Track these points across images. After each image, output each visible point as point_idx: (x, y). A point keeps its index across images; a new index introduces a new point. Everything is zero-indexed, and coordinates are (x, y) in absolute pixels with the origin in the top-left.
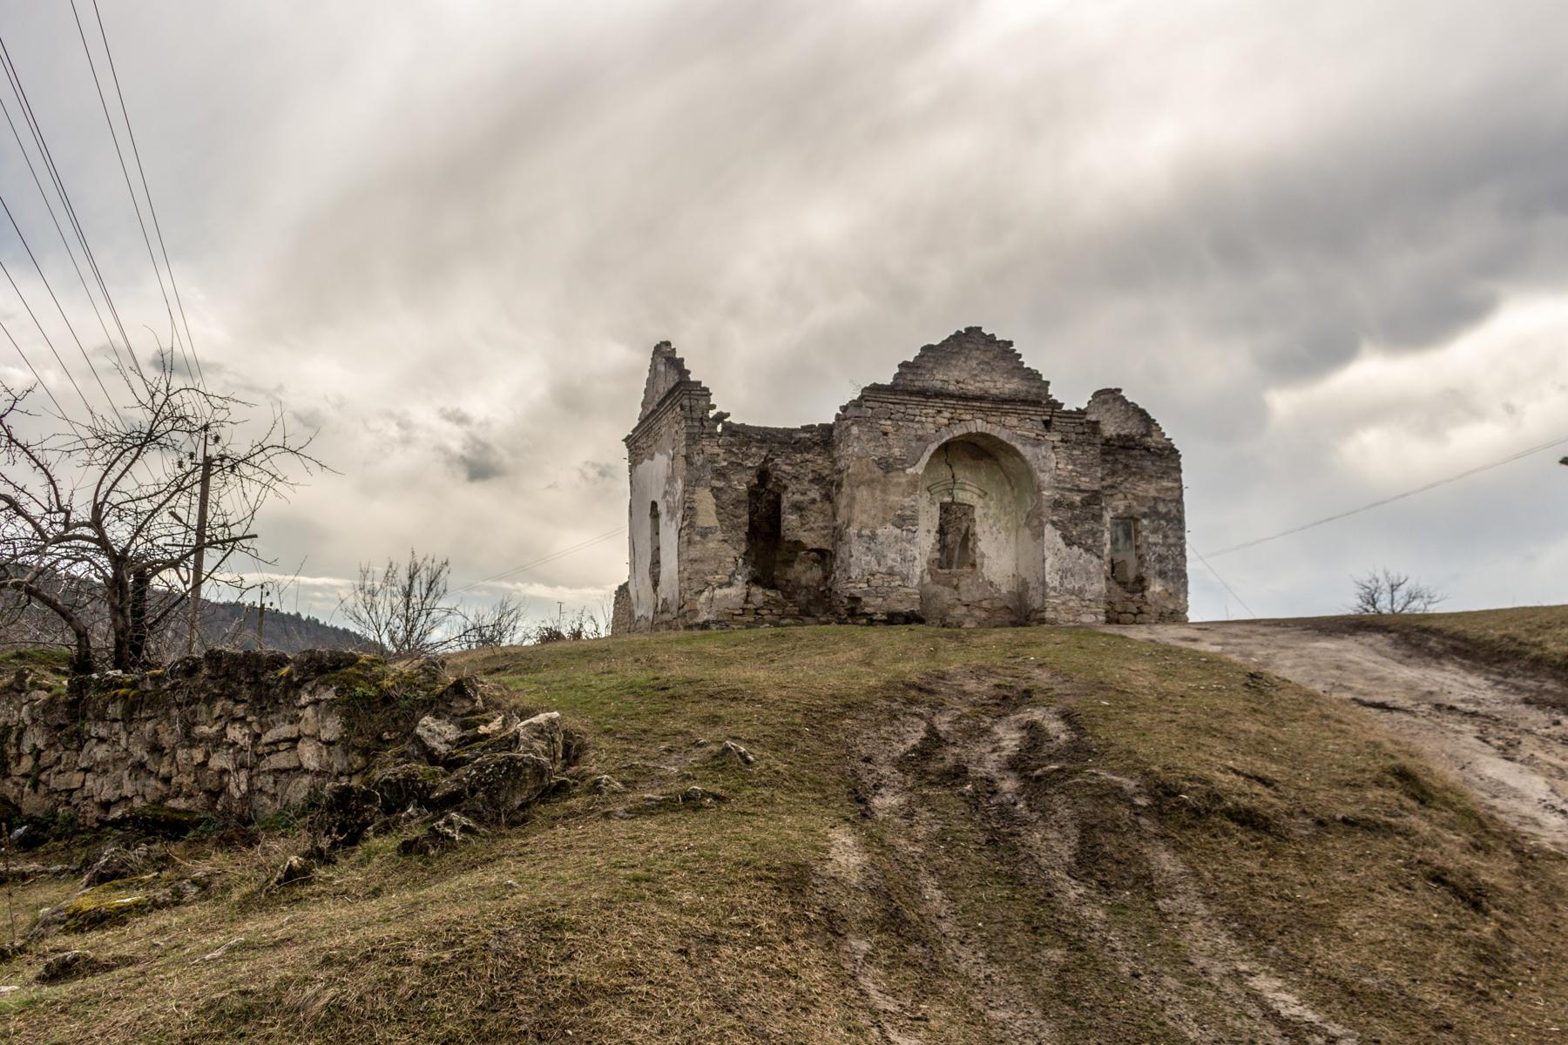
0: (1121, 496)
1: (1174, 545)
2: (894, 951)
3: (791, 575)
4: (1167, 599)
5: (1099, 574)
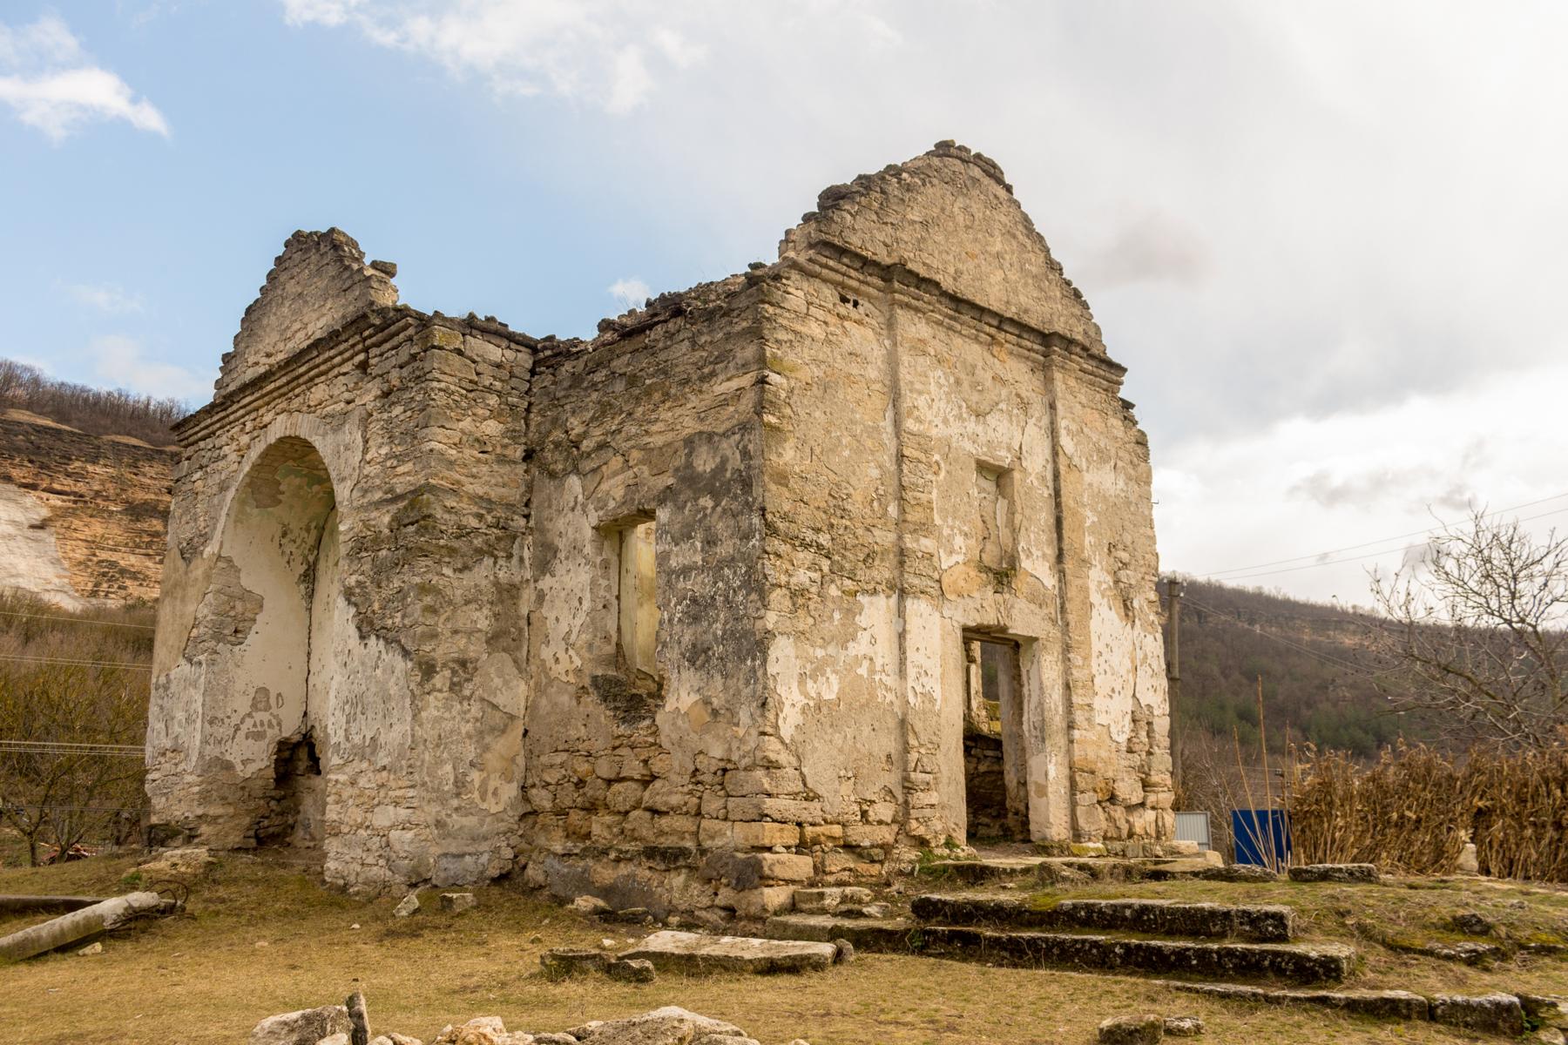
0: (616, 462)
1: (731, 561)
2: (136, 702)
3: (1288, 731)
4: (704, 729)
5: (403, 697)
